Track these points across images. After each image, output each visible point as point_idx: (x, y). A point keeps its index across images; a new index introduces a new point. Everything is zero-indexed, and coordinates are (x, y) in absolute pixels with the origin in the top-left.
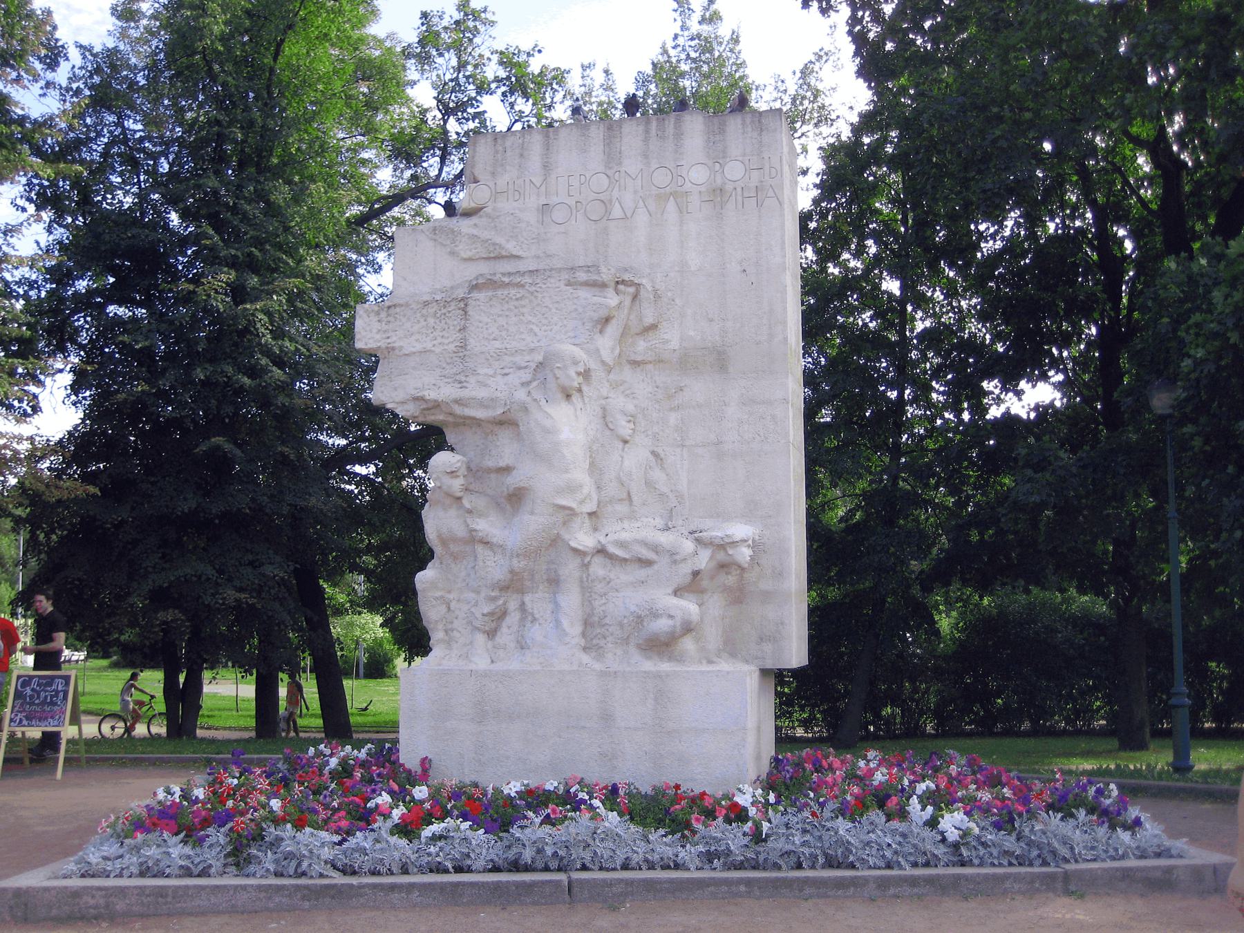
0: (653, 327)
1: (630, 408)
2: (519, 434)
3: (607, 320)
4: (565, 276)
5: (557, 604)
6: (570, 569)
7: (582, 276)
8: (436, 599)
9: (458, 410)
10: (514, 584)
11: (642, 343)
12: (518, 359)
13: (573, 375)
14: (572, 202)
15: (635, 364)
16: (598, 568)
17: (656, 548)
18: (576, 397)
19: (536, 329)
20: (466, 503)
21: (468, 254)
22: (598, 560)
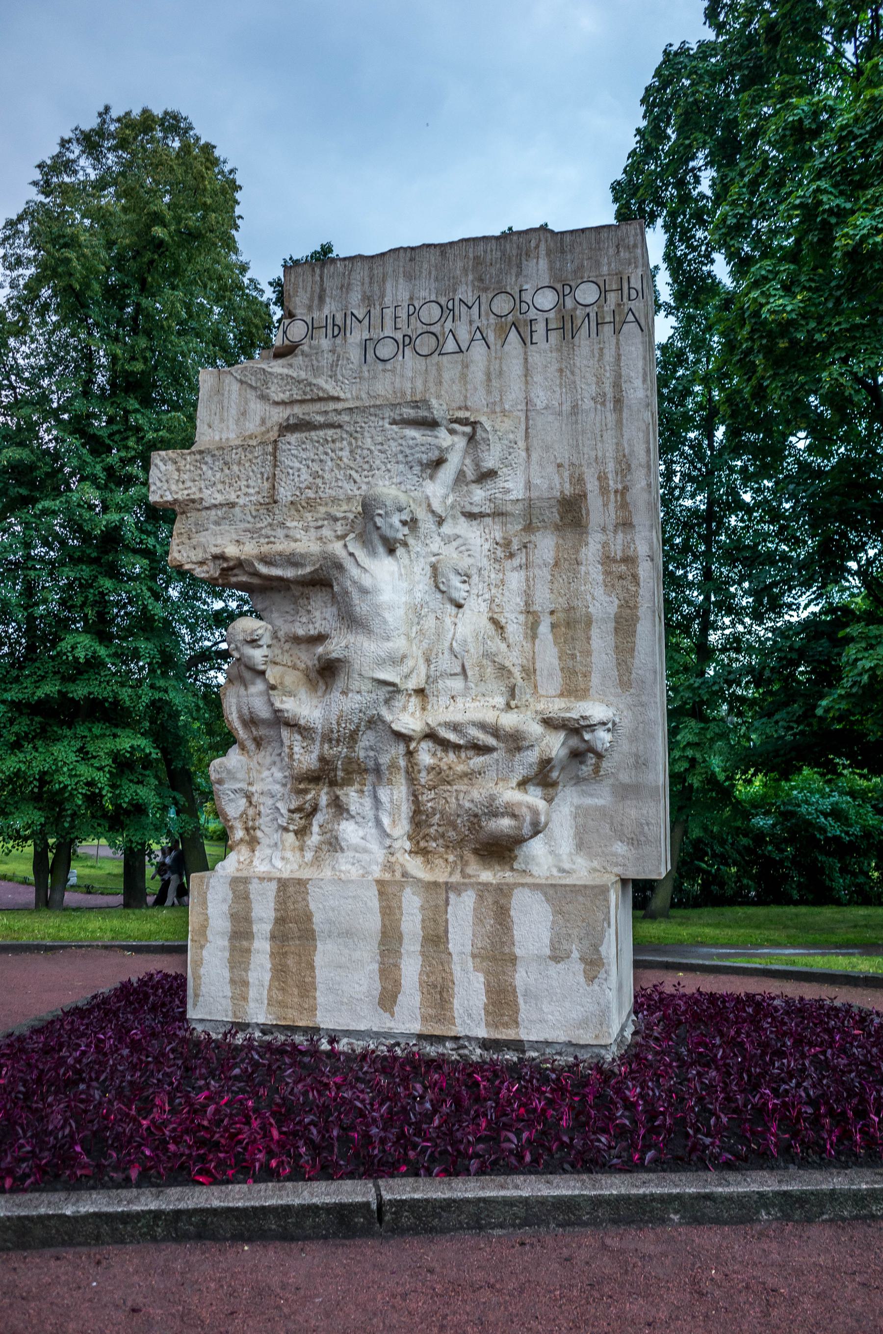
2: (334, 596)
4: (387, 413)
7: (409, 412)
8: (235, 791)
9: (263, 569)
10: (324, 775)
11: (479, 492)
13: (398, 524)
14: (399, 336)
15: (471, 516)
17: (495, 731)
18: (400, 551)
19: (355, 475)
21: (280, 397)
22: (425, 745)
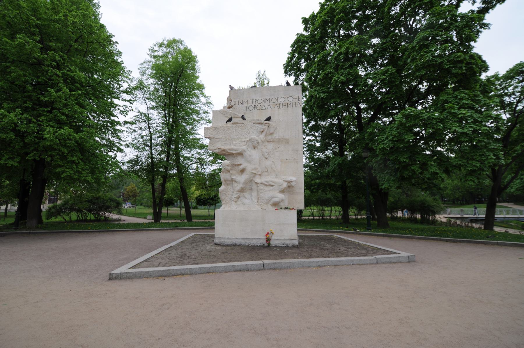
0: (272, 134)
1: (268, 151)
3: (263, 131)
5: (251, 195)
6: (254, 187)
7: (257, 122)
9: (229, 151)
10: (242, 190)
12: (243, 140)
15: (268, 142)
16: (262, 187)
20: (231, 172)
